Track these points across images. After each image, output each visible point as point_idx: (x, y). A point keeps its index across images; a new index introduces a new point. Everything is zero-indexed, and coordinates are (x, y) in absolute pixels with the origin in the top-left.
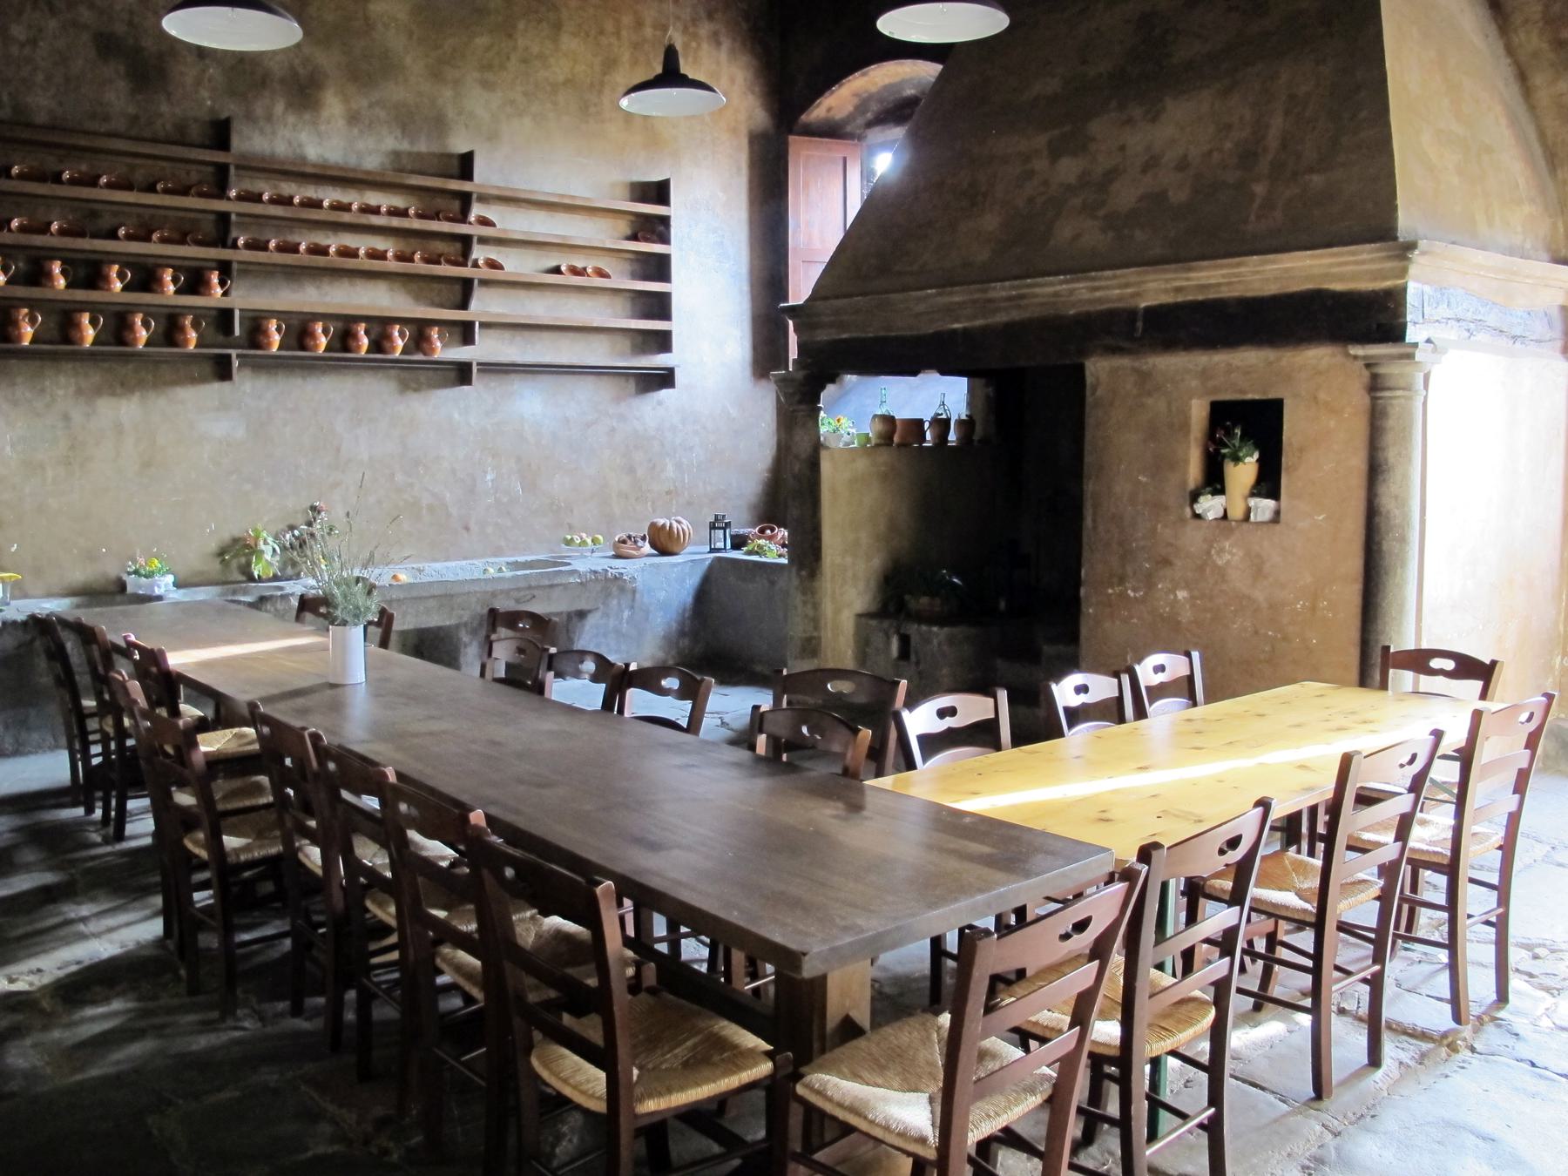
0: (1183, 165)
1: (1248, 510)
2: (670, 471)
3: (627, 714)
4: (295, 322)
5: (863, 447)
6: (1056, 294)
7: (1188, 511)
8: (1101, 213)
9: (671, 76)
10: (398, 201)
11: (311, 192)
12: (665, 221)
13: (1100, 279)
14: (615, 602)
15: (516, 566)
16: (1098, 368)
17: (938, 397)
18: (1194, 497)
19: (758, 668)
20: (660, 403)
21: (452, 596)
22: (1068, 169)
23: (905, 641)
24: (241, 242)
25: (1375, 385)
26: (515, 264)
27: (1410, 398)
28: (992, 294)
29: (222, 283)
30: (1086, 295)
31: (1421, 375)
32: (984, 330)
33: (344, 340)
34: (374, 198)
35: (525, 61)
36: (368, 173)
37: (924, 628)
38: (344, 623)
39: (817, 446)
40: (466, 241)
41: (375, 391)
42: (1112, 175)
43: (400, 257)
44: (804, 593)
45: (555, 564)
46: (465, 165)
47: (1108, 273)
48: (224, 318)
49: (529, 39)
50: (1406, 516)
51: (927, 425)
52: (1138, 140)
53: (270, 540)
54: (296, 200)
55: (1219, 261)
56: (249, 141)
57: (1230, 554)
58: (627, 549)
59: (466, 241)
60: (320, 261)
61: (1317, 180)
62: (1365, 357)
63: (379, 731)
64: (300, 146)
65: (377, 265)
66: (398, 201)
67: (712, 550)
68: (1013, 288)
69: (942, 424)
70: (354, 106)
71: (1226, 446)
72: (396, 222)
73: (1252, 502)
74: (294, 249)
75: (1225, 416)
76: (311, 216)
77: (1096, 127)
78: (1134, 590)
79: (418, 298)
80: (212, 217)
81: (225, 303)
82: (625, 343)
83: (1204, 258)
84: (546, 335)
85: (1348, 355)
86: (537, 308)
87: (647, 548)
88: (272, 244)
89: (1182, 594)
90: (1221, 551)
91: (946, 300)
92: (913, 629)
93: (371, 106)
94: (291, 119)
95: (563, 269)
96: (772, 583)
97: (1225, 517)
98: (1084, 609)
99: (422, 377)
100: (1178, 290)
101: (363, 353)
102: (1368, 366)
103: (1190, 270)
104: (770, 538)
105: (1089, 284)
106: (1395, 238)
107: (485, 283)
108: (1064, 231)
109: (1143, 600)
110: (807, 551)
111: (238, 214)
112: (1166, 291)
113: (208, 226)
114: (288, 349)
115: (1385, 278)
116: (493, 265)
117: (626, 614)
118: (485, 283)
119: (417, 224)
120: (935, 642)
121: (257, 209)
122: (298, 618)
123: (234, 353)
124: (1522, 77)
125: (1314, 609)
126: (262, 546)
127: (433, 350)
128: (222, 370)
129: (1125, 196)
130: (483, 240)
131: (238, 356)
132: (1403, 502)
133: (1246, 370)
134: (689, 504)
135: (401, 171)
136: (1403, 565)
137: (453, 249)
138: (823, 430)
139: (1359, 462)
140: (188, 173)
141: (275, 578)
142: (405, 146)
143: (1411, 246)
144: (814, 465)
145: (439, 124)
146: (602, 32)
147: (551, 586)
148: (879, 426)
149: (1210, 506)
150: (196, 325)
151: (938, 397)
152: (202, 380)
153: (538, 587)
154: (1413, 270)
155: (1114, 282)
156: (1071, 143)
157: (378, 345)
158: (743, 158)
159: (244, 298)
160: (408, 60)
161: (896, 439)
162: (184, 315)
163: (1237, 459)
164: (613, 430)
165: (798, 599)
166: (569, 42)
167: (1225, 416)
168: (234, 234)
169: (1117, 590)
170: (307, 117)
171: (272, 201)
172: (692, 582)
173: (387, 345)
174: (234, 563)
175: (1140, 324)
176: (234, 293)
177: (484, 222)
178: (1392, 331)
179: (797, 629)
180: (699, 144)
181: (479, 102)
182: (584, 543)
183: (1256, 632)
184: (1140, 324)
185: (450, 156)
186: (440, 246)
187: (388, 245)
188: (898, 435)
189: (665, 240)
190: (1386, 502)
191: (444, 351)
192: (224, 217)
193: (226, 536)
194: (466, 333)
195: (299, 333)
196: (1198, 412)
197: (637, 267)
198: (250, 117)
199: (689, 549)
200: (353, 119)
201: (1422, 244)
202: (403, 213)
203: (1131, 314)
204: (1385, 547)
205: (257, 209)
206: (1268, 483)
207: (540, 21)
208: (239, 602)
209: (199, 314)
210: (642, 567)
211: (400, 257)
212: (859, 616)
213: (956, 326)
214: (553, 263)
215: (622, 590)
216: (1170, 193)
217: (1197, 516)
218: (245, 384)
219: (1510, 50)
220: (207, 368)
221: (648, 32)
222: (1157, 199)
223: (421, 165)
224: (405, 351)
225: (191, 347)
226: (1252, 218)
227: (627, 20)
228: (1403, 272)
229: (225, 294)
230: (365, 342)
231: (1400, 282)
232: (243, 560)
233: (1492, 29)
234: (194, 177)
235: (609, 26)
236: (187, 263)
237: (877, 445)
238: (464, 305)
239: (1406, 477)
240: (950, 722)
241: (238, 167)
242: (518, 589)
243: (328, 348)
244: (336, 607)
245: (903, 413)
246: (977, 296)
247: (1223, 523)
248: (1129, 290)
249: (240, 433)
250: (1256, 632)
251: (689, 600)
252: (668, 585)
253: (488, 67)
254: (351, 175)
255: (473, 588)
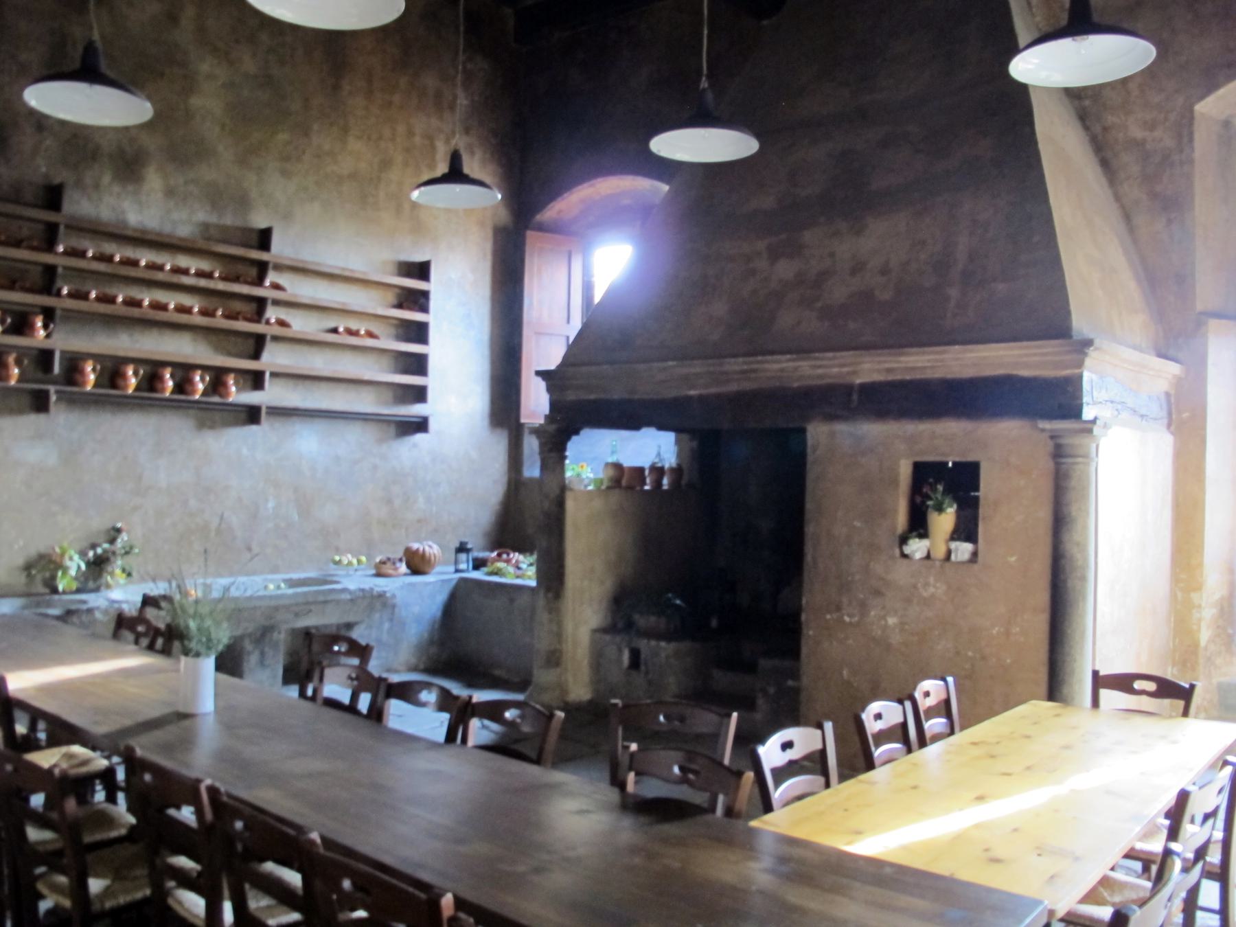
0: (885, 271)
1: (949, 553)
2: (421, 502)
3: (470, 743)
4: (109, 364)
5: (598, 489)
6: (782, 370)
7: (897, 552)
8: (819, 305)
9: (455, 175)
10: (205, 265)
11: (130, 253)
12: (425, 294)
13: (822, 359)
14: (377, 616)
15: (292, 583)
16: (818, 433)
17: (653, 448)
18: (903, 540)
19: (497, 672)
20: (415, 445)
21: (240, 610)
22: (785, 269)
23: (635, 655)
24: (65, 291)
25: (1059, 453)
26: (301, 324)
27: (1088, 464)
28: (727, 368)
29: (46, 326)
30: (809, 372)
31: (1094, 445)
32: (718, 396)
33: (151, 381)
34: (183, 261)
35: (318, 156)
36: (181, 239)
37: (653, 643)
38: (198, 655)
39: (563, 488)
40: (261, 303)
41: (175, 429)
42: (824, 275)
43: (204, 313)
44: (550, 613)
45: (326, 582)
46: (264, 239)
47: (830, 355)
48: (44, 358)
49: (322, 139)
50: (1086, 559)
51: (647, 472)
52: (845, 248)
53: (76, 557)
54: (117, 258)
55: (926, 349)
56: (77, 205)
57: (935, 588)
58: (387, 569)
59: (261, 303)
60: (135, 312)
61: (1001, 287)
62: (1051, 431)
63: (226, 757)
64: (123, 212)
65: (183, 318)
66: (205, 265)
67: (457, 571)
68: (745, 363)
69: (658, 471)
70: (172, 182)
71: (931, 499)
72: (203, 283)
73: (953, 545)
74: (111, 300)
75: (925, 474)
76: (128, 274)
77: (808, 236)
78: (849, 615)
79: (219, 349)
80: (40, 269)
81: (48, 344)
82: (388, 394)
83: (911, 346)
84: (323, 385)
85: (1037, 428)
86: (318, 362)
87: (403, 568)
88: (93, 295)
89: (892, 621)
90: (927, 585)
91: (685, 371)
92: (644, 645)
93: (186, 183)
94: (116, 189)
95: (341, 329)
96: (512, 601)
97: (928, 557)
98: (805, 631)
99: (217, 416)
100: (889, 371)
101: (167, 394)
102: (1052, 437)
103: (901, 355)
104: (508, 561)
105: (813, 363)
106: (1070, 337)
107: (276, 338)
108: (786, 319)
109: (858, 624)
110: (553, 575)
111: (65, 268)
112: (879, 371)
113: (36, 275)
114: (27, 381)
115: (1066, 368)
116: (282, 323)
117: (386, 625)
118: (276, 338)
119: (221, 286)
120: (663, 655)
121: (81, 264)
122: (116, 635)
123: (52, 389)
124: (1127, 217)
125: (1008, 633)
126: (68, 563)
127: (228, 394)
128: (40, 403)
129: (838, 292)
130: (277, 303)
131: (57, 392)
132: (1083, 547)
133: (947, 438)
134: (436, 531)
135: (209, 239)
136: (1084, 598)
137: (249, 308)
138: (568, 474)
139: (1044, 514)
140: (20, 228)
141: (78, 591)
142: (213, 219)
143: (1088, 343)
144: (560, 503)
145: (243, 203)
146: (380, 138)
147: (325, 602)
148: (611, 472)
149: (917, 547)
150: (18, 362)
151: (653, 448)
152: (19, 411)
153: (315, 603)
154: (1088, 362)
155: (836, 362)
156: (793, 249)
157: (182, 386)
158: (488, 246)
159: (64, 341)
160: (221, 148)
161: (624, 482)
162: (8, 353)
163: (940, 509)
164: (375, 467)
165: (543, 616)
166: (354, 144)
167: (925, 474)
168: (59, 283)
169: (835, 616)
170: (130, 188)
171: (94, 258)
172: (441, 597)
173: (188, 388)
174: (39, 578)
175: (855, 397)
176: (55, 336)
177: (276, 287)
178: (1073, 411)
179: (542, 643)
180: (454, 233)
181: (278, 187)
182: (350, 563)
183: (958, 653)
184: (855, 397)
185: (251, 230)
186: (238, 306)
187: (195, 304)
188: (623, 479)
189: (424, 309)
190: (1070, 548)
191: (237, 395)
192: (50, 270)
193: (33, 551)
194: (256, 380)
195: (112, 373)
196: (905, 471)
197: (400, 331)
198: (79, 184)
199: (438, 569)
200: (170, 193)
201: (1097, 342)
202: (209, 276)
203: (848, 389)
204: (1070, 584)
205: (81, 264)
206: (966, 530)
207: (331, 124)
208: (46, 616)
209: (22, 353)
210: (398, 584)
211: (204, 313)
212: (595, 631)
213: (692, 393)
214: (332, 325)
215: (384, 605)
216: (877, 293)
217: (904, 556)
218: (61, 418)
219: (1117, 198)
220: (26, 400)
221: (417, 140)
222: (866, 298)
223: (226, 235)
224: (205, 394)
225: (13, 382)
226: (949, 315)
227: (401, 129)
228: (1080, 364)
229: (48, 336)
230: (170, 384)
231: (1076, 371)
232: (47, 574)
233: (1104, 181)
234: (25, 232)
235: (387, 132)
236: (15, 308)
237: (609, 488)
238: (256, 355)
239: (1085, 527)
240: (792, 754)
241: (68, 227)
242: (297, 605)
243: (137, 389)
244: (190, 640)
245: (629, 462)
246: (712, 369)
247: (926, 562)
248: (845, 370)
249: (52, 460)
250: (958, 653)
251: (439, 614)
252: (420, 600)
253: (287, 159)
254: (167, 240)
255: (258, 603)
